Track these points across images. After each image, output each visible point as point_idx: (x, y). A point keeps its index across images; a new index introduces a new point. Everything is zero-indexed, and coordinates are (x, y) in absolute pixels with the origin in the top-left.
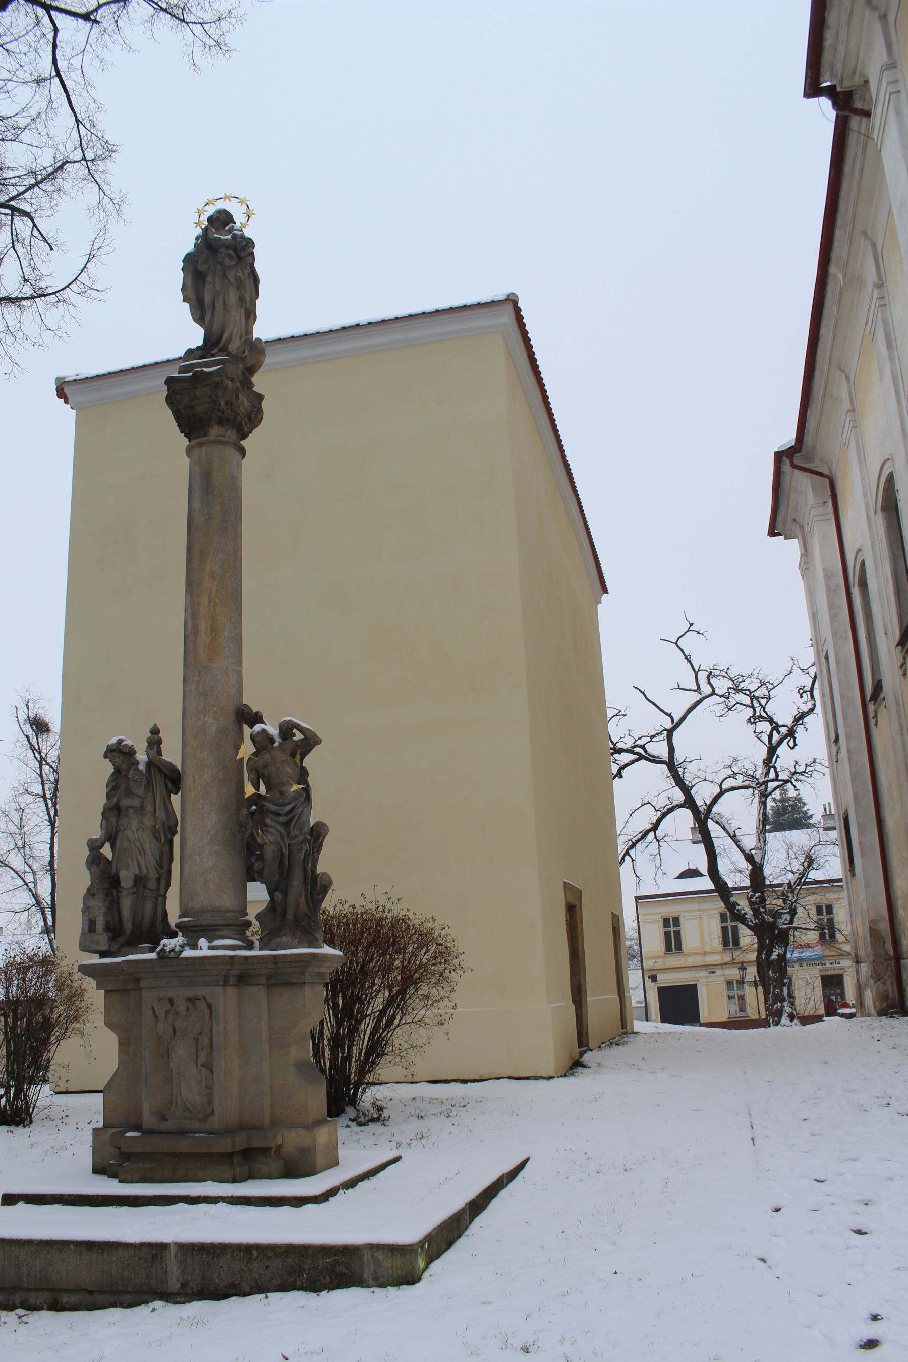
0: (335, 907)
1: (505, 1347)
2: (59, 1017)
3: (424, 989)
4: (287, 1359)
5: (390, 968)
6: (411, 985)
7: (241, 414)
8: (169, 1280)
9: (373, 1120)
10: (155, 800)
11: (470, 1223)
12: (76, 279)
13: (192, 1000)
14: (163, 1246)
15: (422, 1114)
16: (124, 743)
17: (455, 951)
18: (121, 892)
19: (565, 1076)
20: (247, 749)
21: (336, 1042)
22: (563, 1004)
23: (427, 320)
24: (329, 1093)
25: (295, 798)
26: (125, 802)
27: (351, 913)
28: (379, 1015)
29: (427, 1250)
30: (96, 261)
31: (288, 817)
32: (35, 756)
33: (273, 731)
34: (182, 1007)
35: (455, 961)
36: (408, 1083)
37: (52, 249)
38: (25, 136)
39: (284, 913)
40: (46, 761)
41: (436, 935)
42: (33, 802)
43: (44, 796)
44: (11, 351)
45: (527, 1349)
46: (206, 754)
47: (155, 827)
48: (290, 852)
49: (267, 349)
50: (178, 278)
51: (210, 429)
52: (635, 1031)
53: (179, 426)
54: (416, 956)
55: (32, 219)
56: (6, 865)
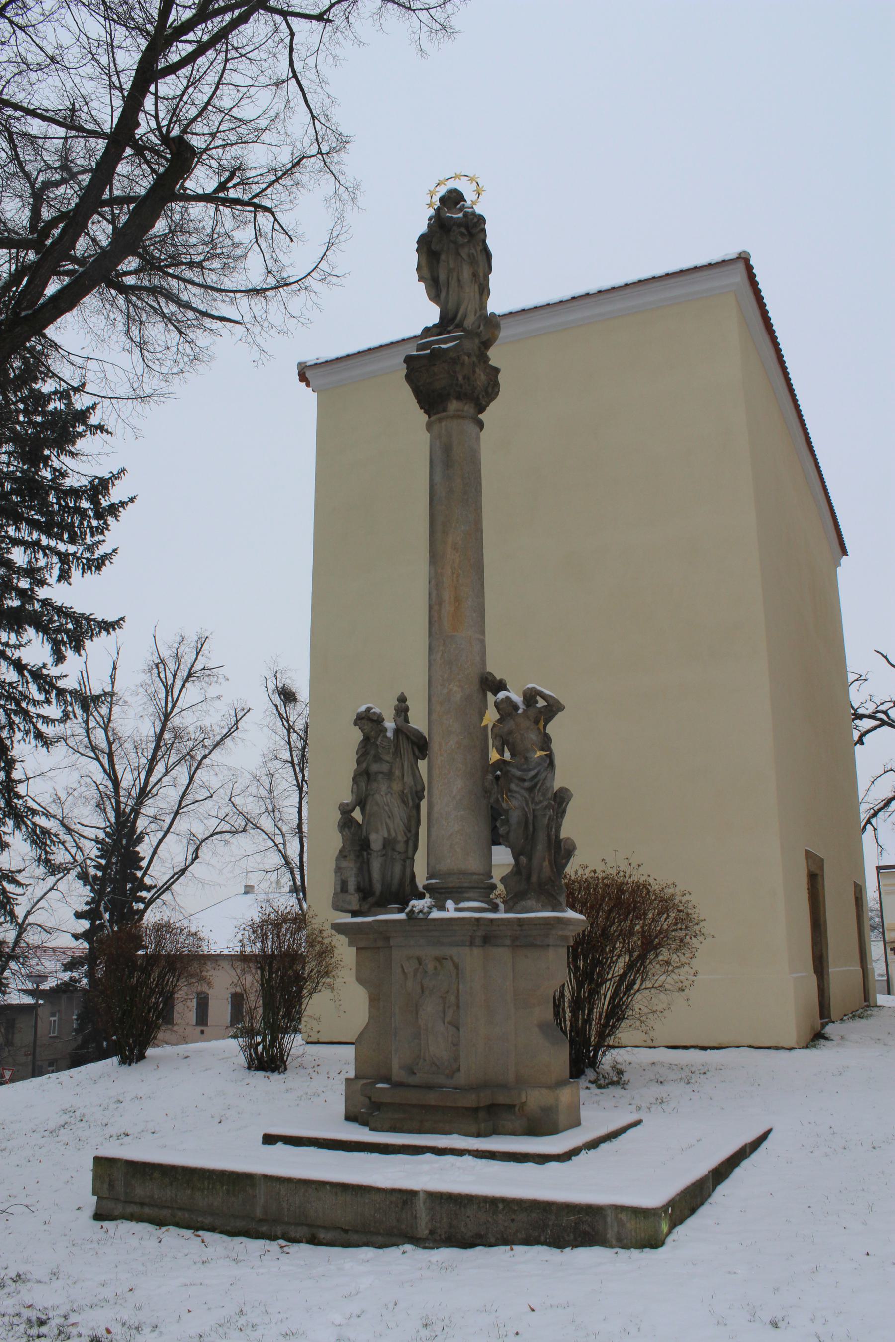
0: (576, 872)
1: (753, 1319)
2: (311, 971)
3: (664, 955)
4: (533, 1310)
5: (631, 933)
6: (651, 950)
7: (479, 388)
8: (418, 1225)
9: (612, 1083)
11: (713, 1190)
12: (317, 267)
13: (439, 960)
14: (413, 1194)
15: (661, 1079)
16: (372, 711)
17: (696, 918)
18: (371, 854)
19: (807, 1047)
20: (491, 716)
21: (577, 1004)
22: (805, 974)
23: (658, 284)
24: (571, 1054)
25: (539, 764)
26: (375, 768)
27: (592, 878)
28: (619, 980)
29: (671, 1215)
30: (335, 249)
31: (533, 783)
32: (283, 724)
33: (517, 698)
34: (430, 966)
35: (696, 927)
36: (646, 1047)
37: (292, 240)
38: (266, 137)
39: (528, 878)
40: (294, 729)
41: (676, 901)
42: (282, 768)
43: (292, 763)
44: (259, 340)
45: (776, 1324)
46: (452, 720)
47: (403, 792)
48: (534, 817)
49: (502, 322)
50: (412, 258)
51: (449, 404)
52: (878, 1004)
53: (419, 402)
54: (657, 921)
55: (273, 214)
56: (258, 827)
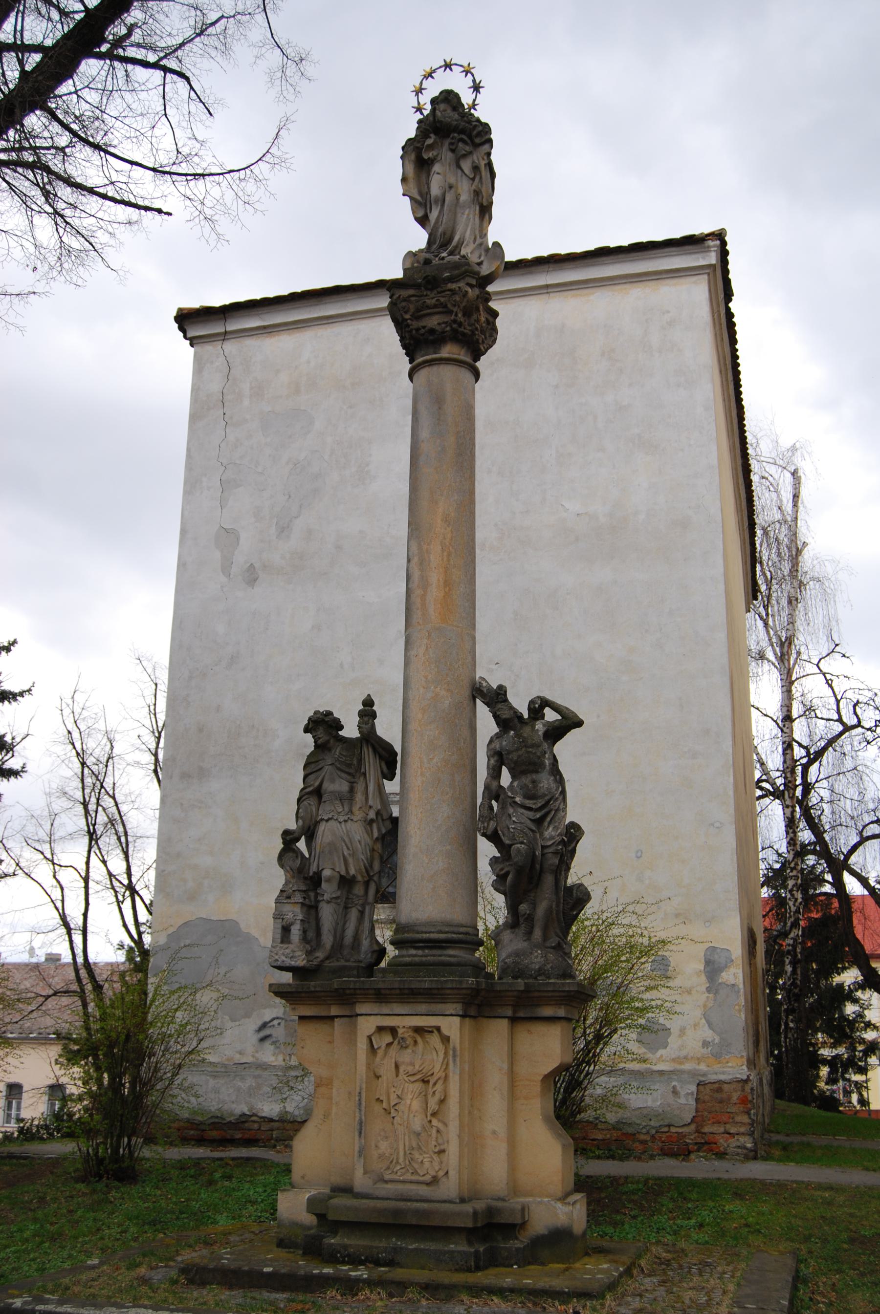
10: (367, 787)
31: (543, 812)
